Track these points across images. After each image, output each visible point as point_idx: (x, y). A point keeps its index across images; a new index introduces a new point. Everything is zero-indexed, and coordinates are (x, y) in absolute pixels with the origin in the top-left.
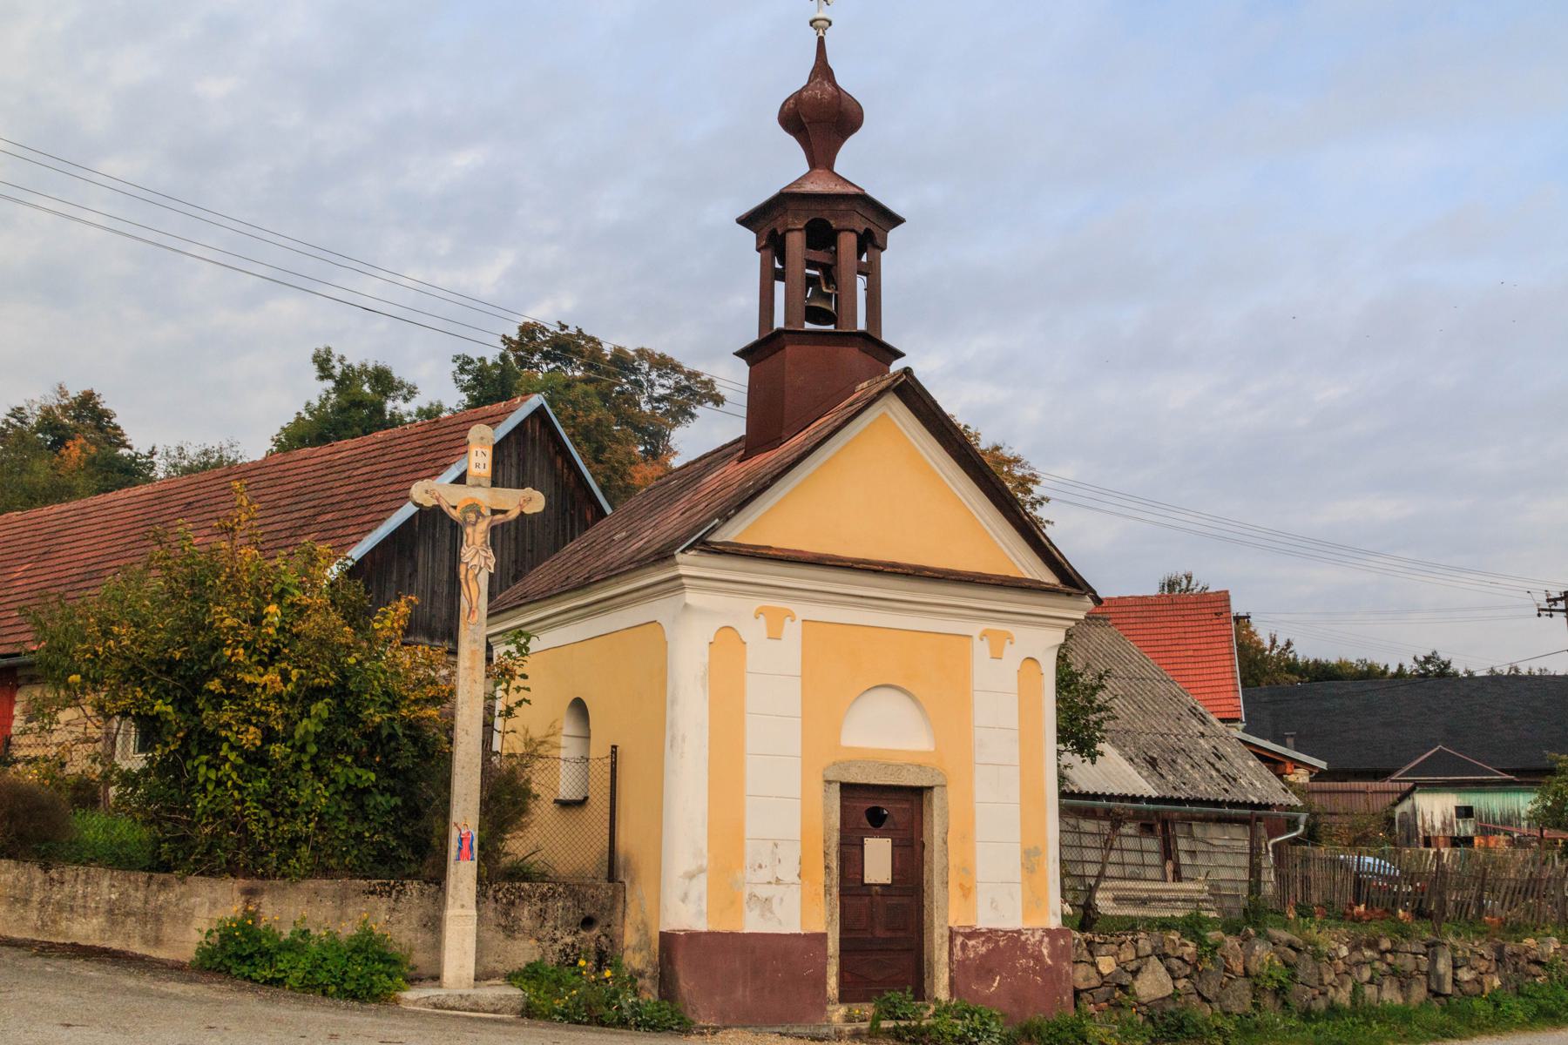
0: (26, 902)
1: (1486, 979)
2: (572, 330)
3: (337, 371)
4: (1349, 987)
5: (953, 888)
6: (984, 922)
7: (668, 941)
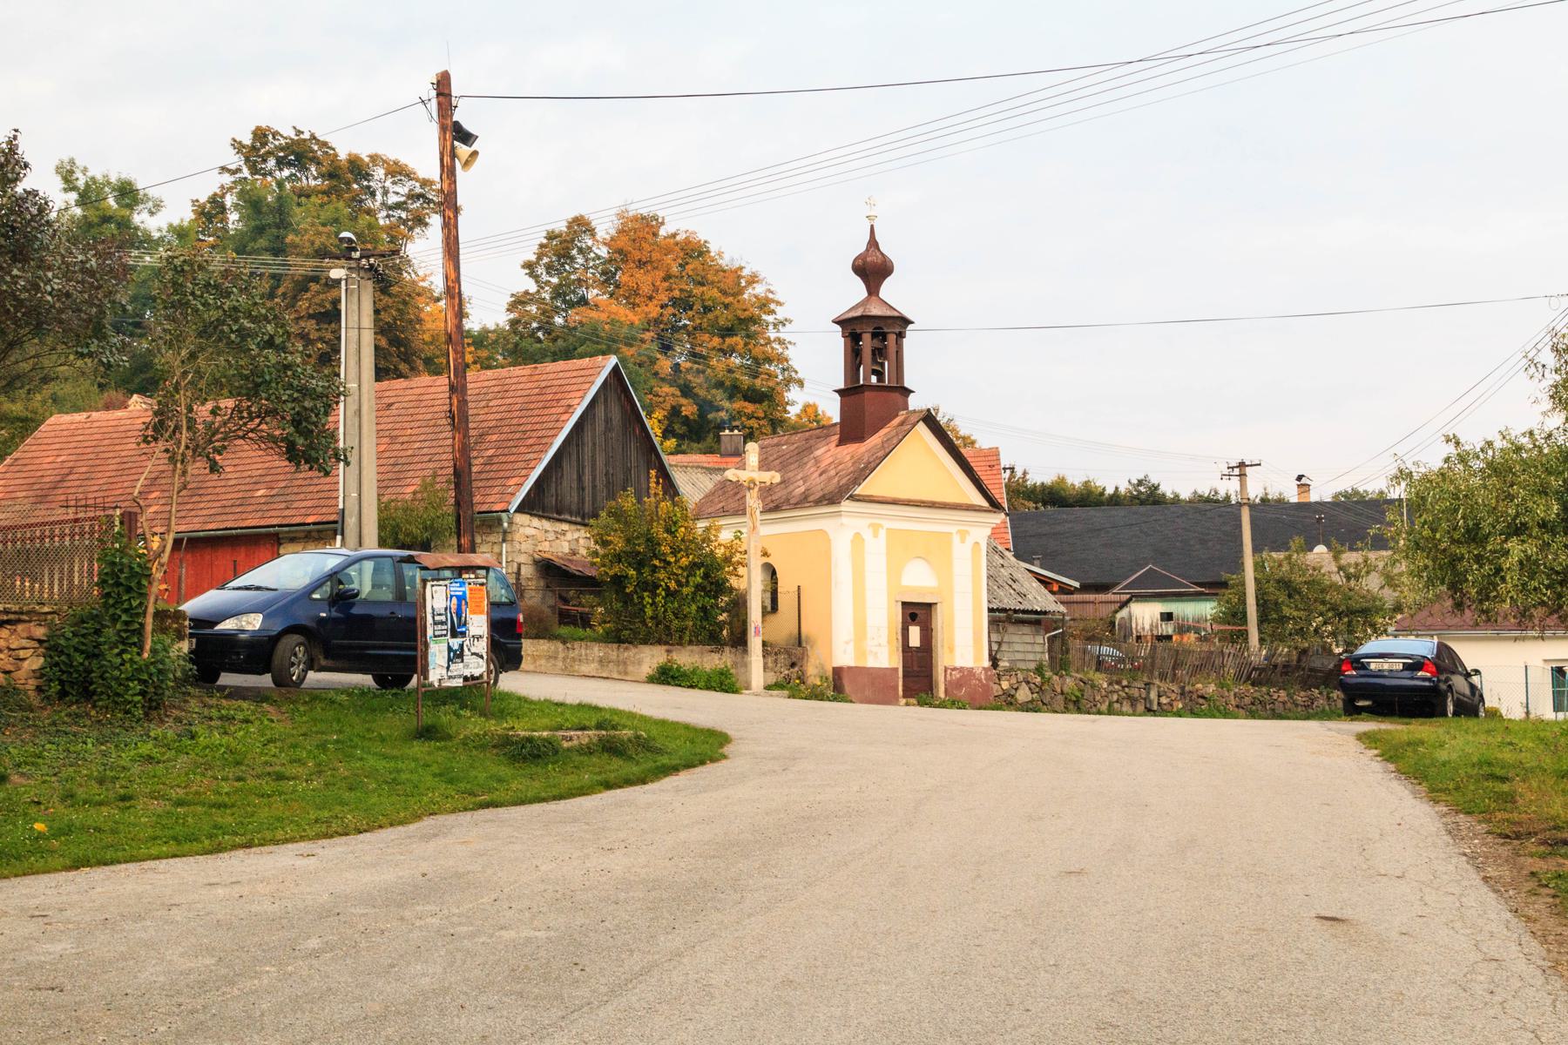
0: (556, 658)
1: (1175, 704)
2: (306, 136)
3: (81, 183)
4: (1107, 703)
5: (946, 649)
6: (958, 664)
7: (838, 672)
